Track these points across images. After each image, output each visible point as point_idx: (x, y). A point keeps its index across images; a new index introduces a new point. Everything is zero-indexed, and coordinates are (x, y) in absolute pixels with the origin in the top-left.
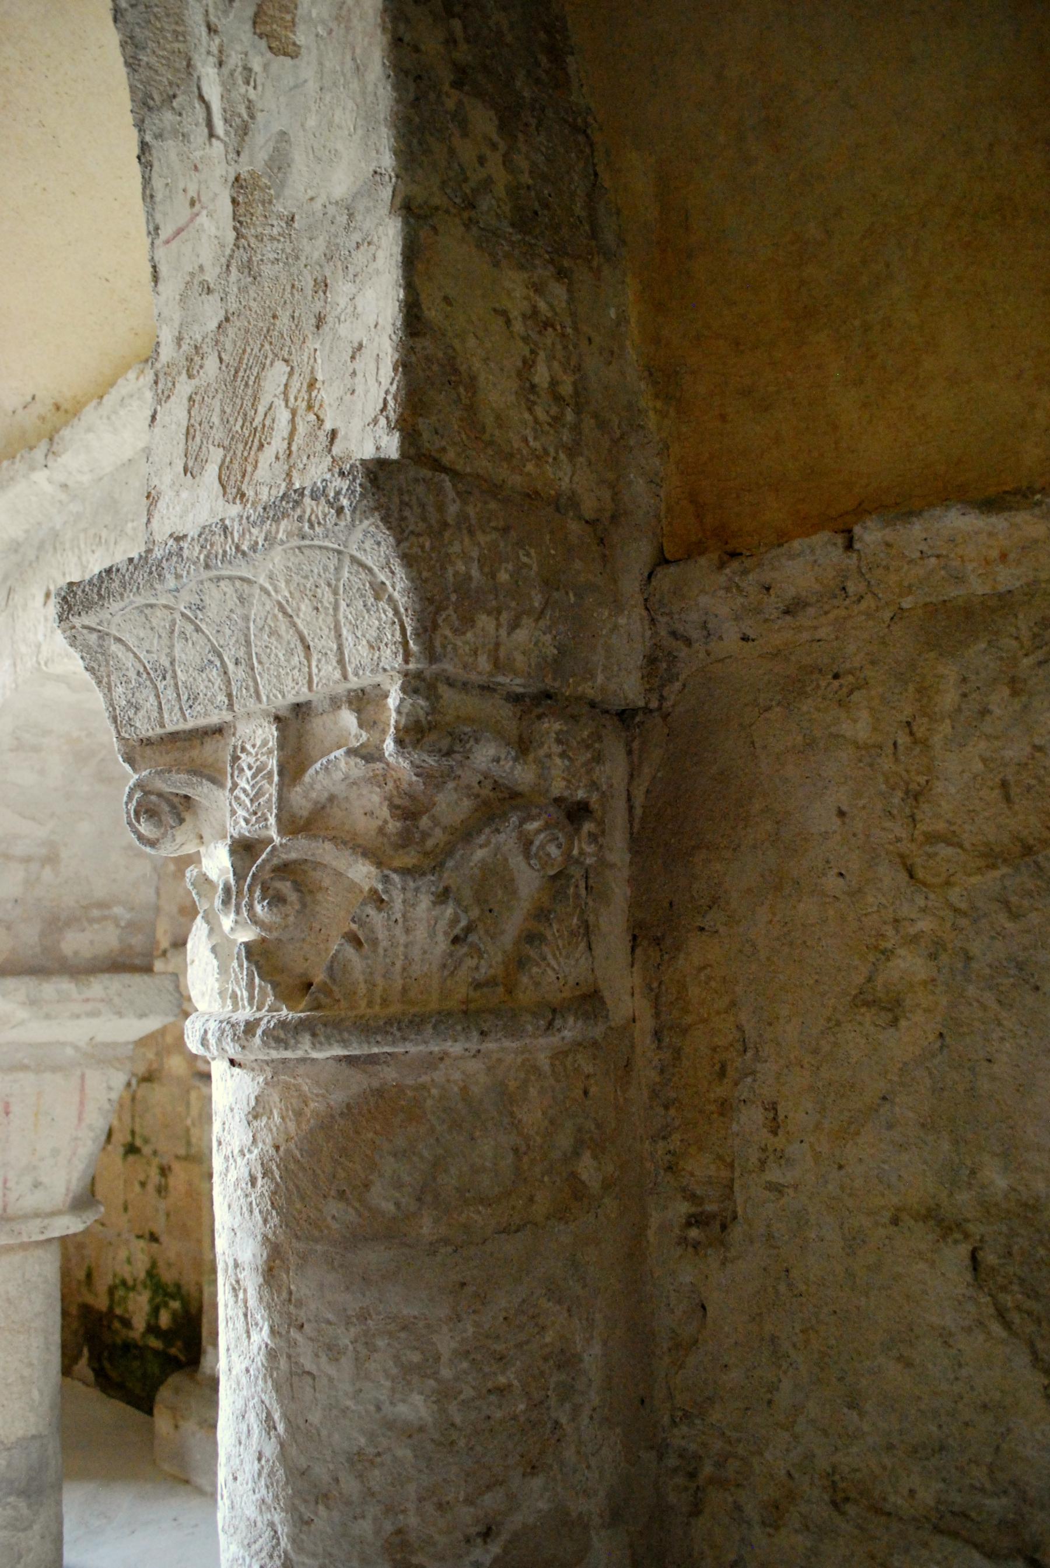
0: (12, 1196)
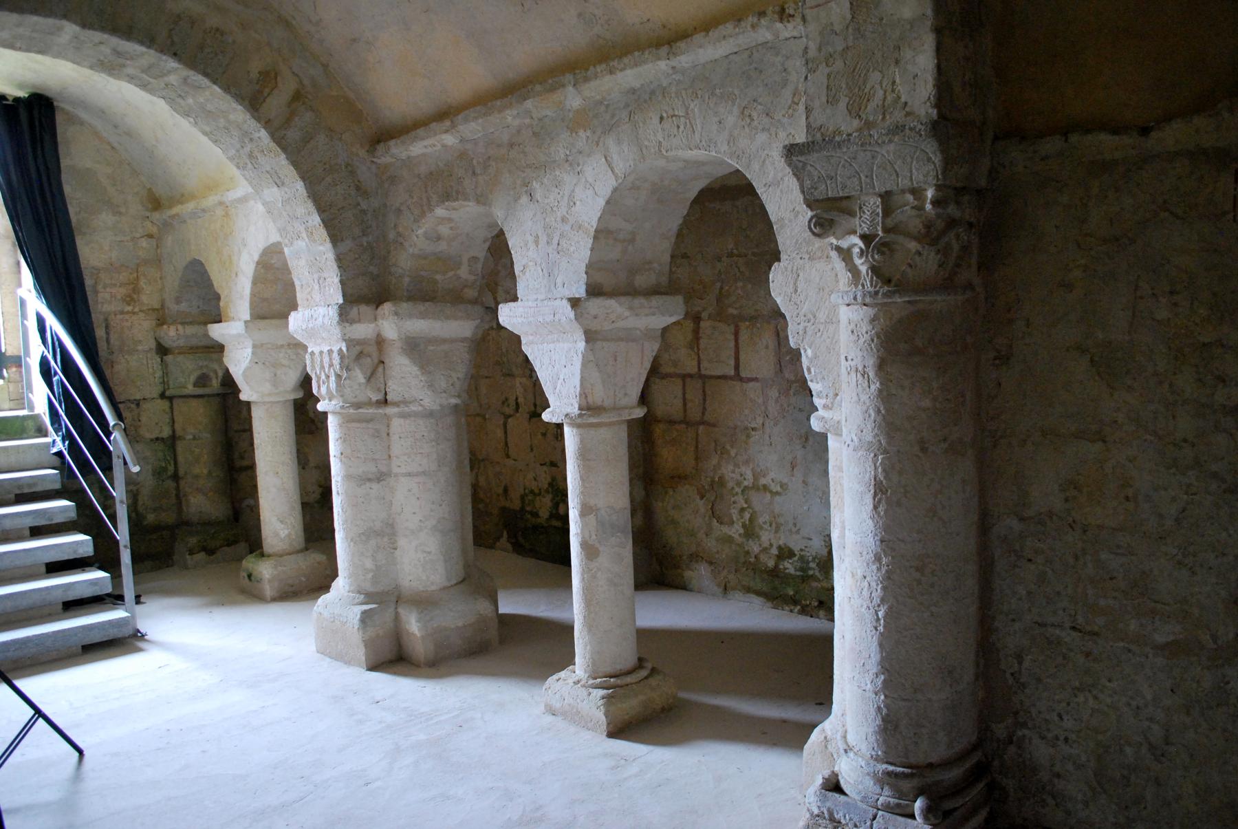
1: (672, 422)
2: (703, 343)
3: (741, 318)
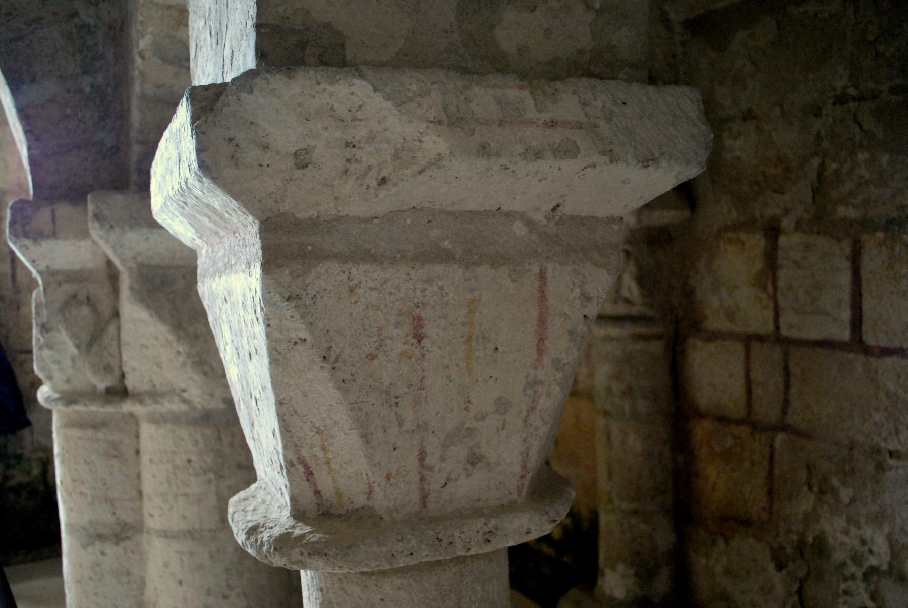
0: (436, 481)
1: (723, 420)
2: (784, 276)
3: (867, 225)
